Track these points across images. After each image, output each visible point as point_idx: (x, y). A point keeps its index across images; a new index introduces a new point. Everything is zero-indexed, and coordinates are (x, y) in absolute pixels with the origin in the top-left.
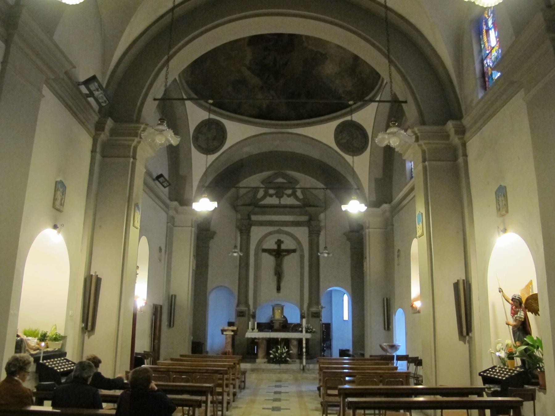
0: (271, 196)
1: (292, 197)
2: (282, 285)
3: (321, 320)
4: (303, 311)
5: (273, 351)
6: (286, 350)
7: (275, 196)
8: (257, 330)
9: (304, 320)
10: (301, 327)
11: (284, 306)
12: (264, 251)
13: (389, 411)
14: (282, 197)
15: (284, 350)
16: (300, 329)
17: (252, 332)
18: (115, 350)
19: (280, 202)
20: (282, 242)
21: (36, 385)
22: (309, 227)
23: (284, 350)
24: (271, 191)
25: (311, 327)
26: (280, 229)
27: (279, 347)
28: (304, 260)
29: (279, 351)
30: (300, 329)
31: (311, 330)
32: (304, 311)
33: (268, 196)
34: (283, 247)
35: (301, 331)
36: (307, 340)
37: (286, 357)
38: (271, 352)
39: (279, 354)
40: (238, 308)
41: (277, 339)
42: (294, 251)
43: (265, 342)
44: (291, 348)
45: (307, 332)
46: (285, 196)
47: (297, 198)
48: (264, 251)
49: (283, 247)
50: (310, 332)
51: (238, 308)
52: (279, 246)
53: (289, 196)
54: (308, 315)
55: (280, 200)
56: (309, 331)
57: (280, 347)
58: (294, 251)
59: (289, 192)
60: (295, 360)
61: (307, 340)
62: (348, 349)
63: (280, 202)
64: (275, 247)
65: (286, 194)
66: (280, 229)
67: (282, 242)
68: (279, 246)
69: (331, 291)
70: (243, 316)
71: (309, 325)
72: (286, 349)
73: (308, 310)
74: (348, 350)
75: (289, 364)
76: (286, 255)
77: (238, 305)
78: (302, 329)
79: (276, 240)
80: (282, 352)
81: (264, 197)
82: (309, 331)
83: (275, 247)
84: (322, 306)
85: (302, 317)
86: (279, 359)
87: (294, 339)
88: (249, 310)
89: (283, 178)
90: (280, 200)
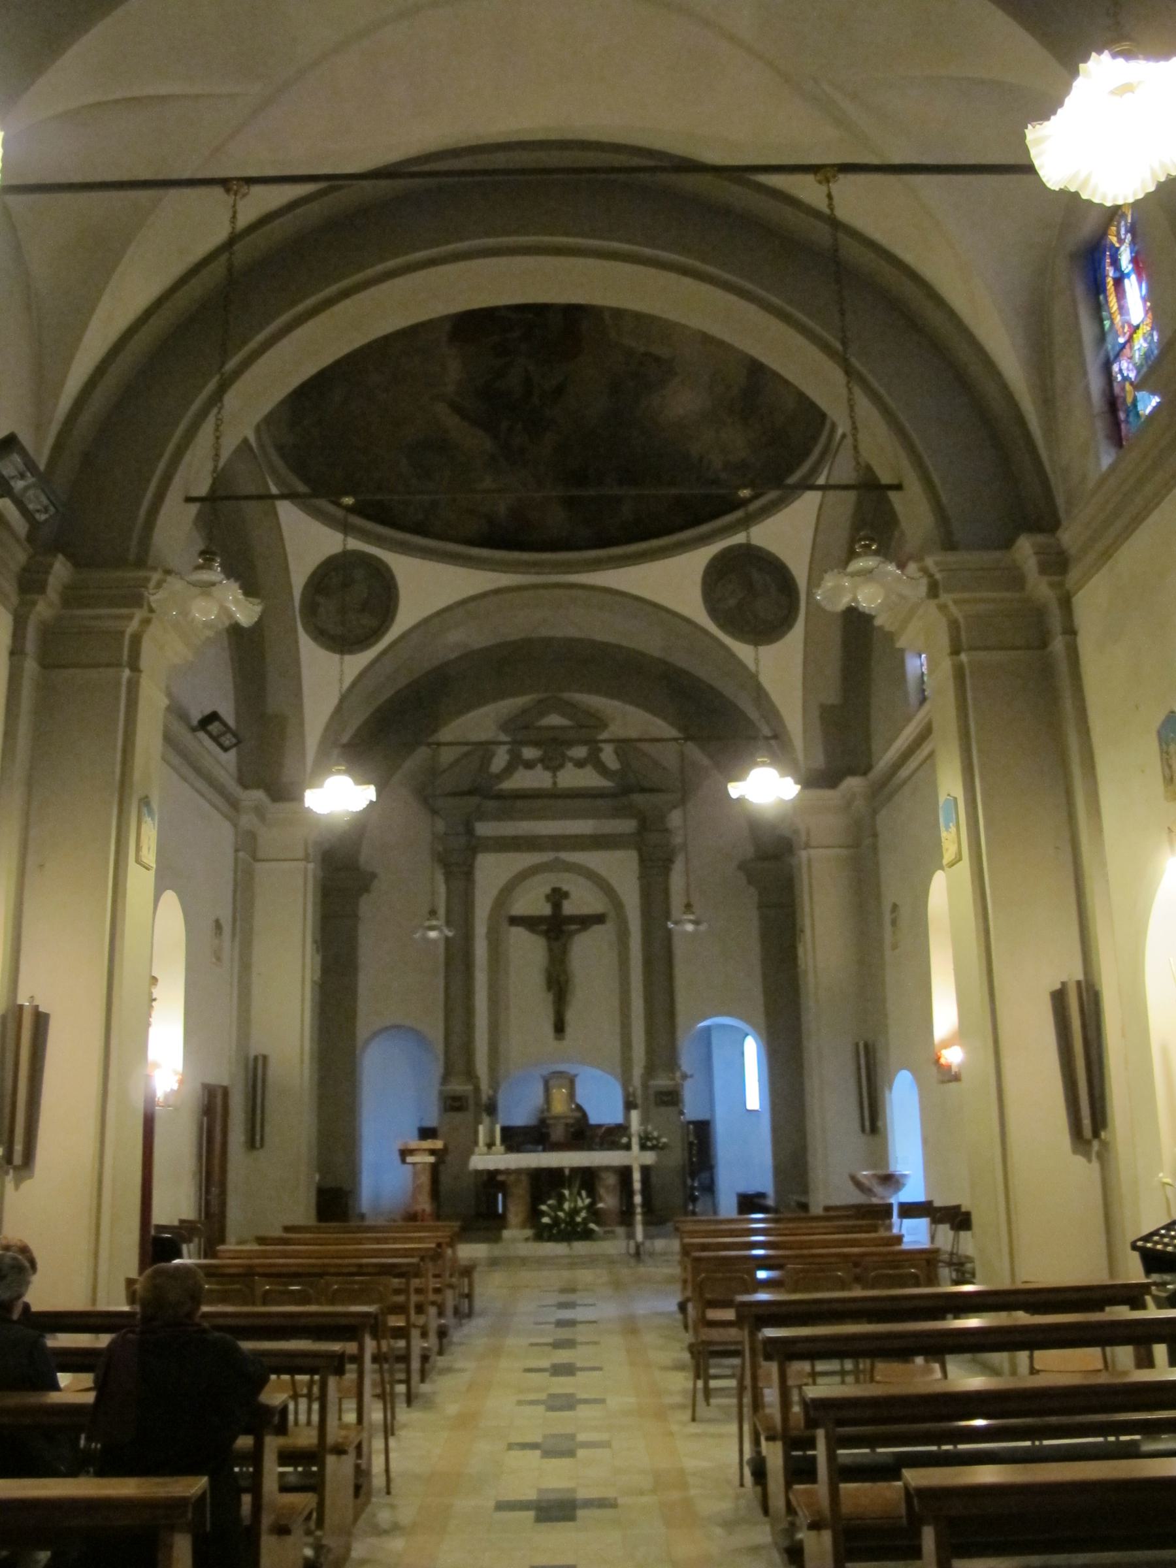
0: (529, 765)
2: (570, 1016)
3: (682, 1113)
5: (549, 1206)
6: (588, 1201)
9: (635, 1115)
12: (515, 921)
19: (555, 783)
20: (566, 895)
24: (529, 753)
25: (655, 1134)
26: (557, 859)
27: (566, 1192)
29: (566, 1206)
30: (624, 1140)
34: (568, 908)
35: (628, 1147)
37: (585, 1221)
42: (599, 919)
43: (524, 1179)
45: (643, 1147)
46: (570, 765)
48: (515, 921)
49: (568, 908)
50: (652, 1148)
51: (443, 1088)
52: (557, 906)
53: (580, 764)
55: (555, 776)
58: (599, 919)
59: (580, 752)
64: (546, 910)
65: (571, 759)
66: (557, 859)
68: (557, 906)
69: (708, 1029)
73: (645, 1086)
77: (446, 1078)
81: (509, 770)
83: (546, 910)
85: (629, 1105)
86: (566, 1228)
87: (608, 1168)
88: (477, 1089)
90: (555, 776)
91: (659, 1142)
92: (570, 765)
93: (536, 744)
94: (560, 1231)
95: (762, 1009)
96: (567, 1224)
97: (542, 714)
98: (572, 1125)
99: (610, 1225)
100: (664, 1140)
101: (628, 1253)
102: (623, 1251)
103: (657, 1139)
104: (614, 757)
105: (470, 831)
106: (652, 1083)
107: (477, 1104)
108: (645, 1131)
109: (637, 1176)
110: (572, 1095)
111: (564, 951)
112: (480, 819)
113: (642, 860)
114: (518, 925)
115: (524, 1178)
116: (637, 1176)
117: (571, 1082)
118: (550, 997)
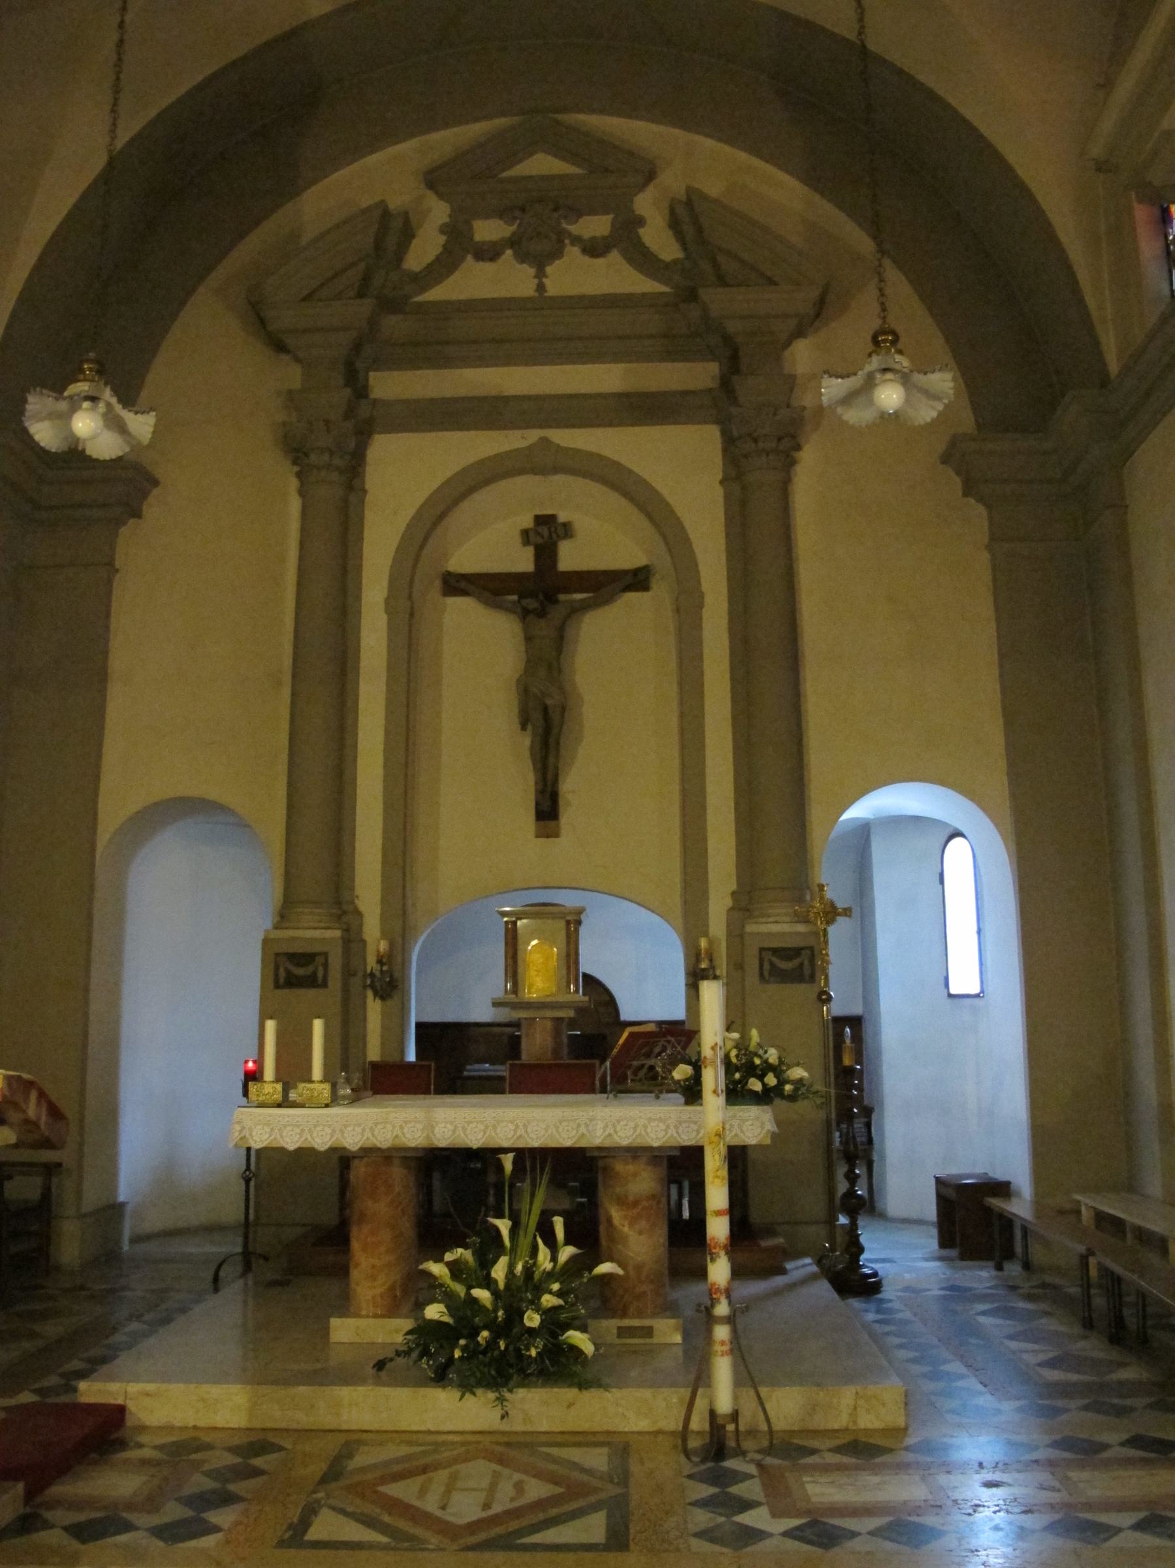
0: (488, 253)
1: (615, 256)
2: (570, 785)
3: (824, 998)
4: (703, 943)
5: (452, 1265)
6: (567, 1252)
7: (509, 252)
8: (325, 1090)
9: (712, 994)
10: (691, 1052)
11: (580, 911)
12: (456, 584)
13: (532, 747)
14: (556, 253)
15: (544, 1253)
16: (681, 1072)
17: (284, 1103)
18: (983, 953)
19: (541, 288)
20: (567, 531)
21: (370, 1093)
22: (723, 422)
23: (544, 1253)
24: (487, 230)
25: (772, 1055)
26: (544, 441)
27: (503, 1226)
28: (698, 626)
29: (499, 1272)
30: (681, 1072)
31: (771, 1080)
32: (711, 943)
33: (469, 258)
34: (570, 558)
35: (692, 1092)
36: (737, 1157)
37: (555, 1323)
38: (437, 1269)
39: (496, 1294)
40: (280, 934)
41: (488, 1156)
42: (638, 580)
43: (399, 1177)
44: (609, 1220)
45: (735, 1094)
46: (573, 252)
47: (643, 259)
48: (456, 584)
49: (570, 558)
50: (764, 1097)
51: (280, 934)
52: (546, 554)
53: (594, 249)
54: (738, 966)
55: (541, 274)
56: (755, 1085)
57: (514, 1231)
58: (638, 580)
59: (597, 226)
60: (647, 1322)
61: (737, 1157)
62: (999, 1175)
63: (541, 288)
64: (523, 561)
65: (576, 240)
66: (544, 441)
67: (567, 531)
68: (546, 554)
69: (864, 830)
70: (311, 982)
71: (754, 1034)
72: (568, 1241)
73: (736, 935)
74: (1002, 1189)
75: (583, 1385)
76: (585, 607)
77: (283, 917)
78: (697, 1067)
79: (527, 521)
80: (529, 1272)
81: (444, 266)
82: (755, 1085)
83: (523, 561)
84: (832, 905)
85: (696, 976)
86: (492, 1343)
87: (634, 1152)
88: (352, 940)
89: (559, 152)
90: (541, 274)
91: (781, 1083)
92: (573, 252)
93: (503, 213)
94: (472, 1353)
95: (1002, 764)
96: (498, 1331)
97: (514, 158)
98: (572, 1023)
99: (640, 1315)
100: (797, 1073)
101: (685, 1433)
102: (673, 1423)
103: (777, 1070)
104: (668, 235)
105: (361, 392)
106: (750, 928)
107: (348, 973)
108: (742, 1046)
109: (715, 1167)
110: (571, 956)
111: (560, 641)
112: (379, 363)
113: (729, 441)
114: (464, 593)
115: (398, 1174)
116: (715, 1167)
117: (573, 923)
118: (526, 741)
